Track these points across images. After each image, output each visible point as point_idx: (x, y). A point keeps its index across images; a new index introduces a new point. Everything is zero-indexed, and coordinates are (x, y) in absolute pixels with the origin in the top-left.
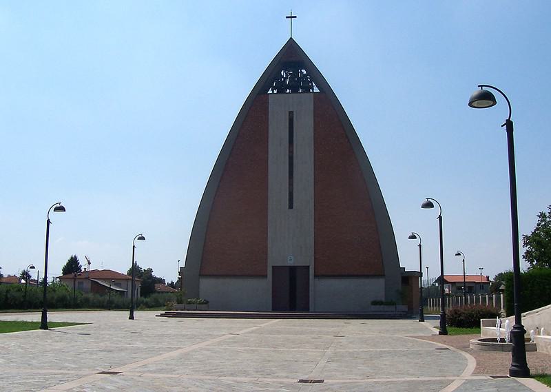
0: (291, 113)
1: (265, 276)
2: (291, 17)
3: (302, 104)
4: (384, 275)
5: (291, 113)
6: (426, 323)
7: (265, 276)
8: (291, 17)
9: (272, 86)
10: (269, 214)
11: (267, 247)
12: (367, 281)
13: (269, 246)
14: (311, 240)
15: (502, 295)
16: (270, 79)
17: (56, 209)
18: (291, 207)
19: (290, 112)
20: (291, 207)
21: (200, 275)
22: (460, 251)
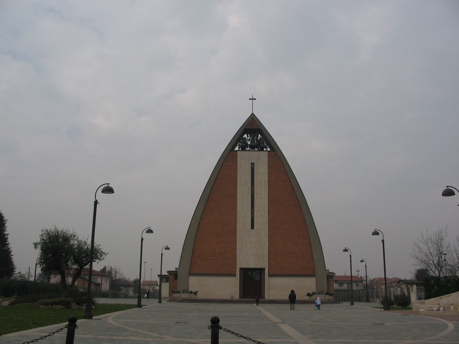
0: (253, 164)
1: (235, 275)
2: (253, 99)
3: (261, 158)
4: (315, 275)
5: (253, 164)
6: (323, 295)
7: (235, 275)
8: (253, 99)
9: (240, 142)
10: (238, 231)
11: (236, 255)
12: (304, 279)
13: (238, 253)
14: (266, 251)
15: (420, 310)
16: (238, 139)
17: (147, 232)
18: (252, 227)
19: (252, 163)
20: (252, 227)
21: (189, 274)
22: (363, 259)
